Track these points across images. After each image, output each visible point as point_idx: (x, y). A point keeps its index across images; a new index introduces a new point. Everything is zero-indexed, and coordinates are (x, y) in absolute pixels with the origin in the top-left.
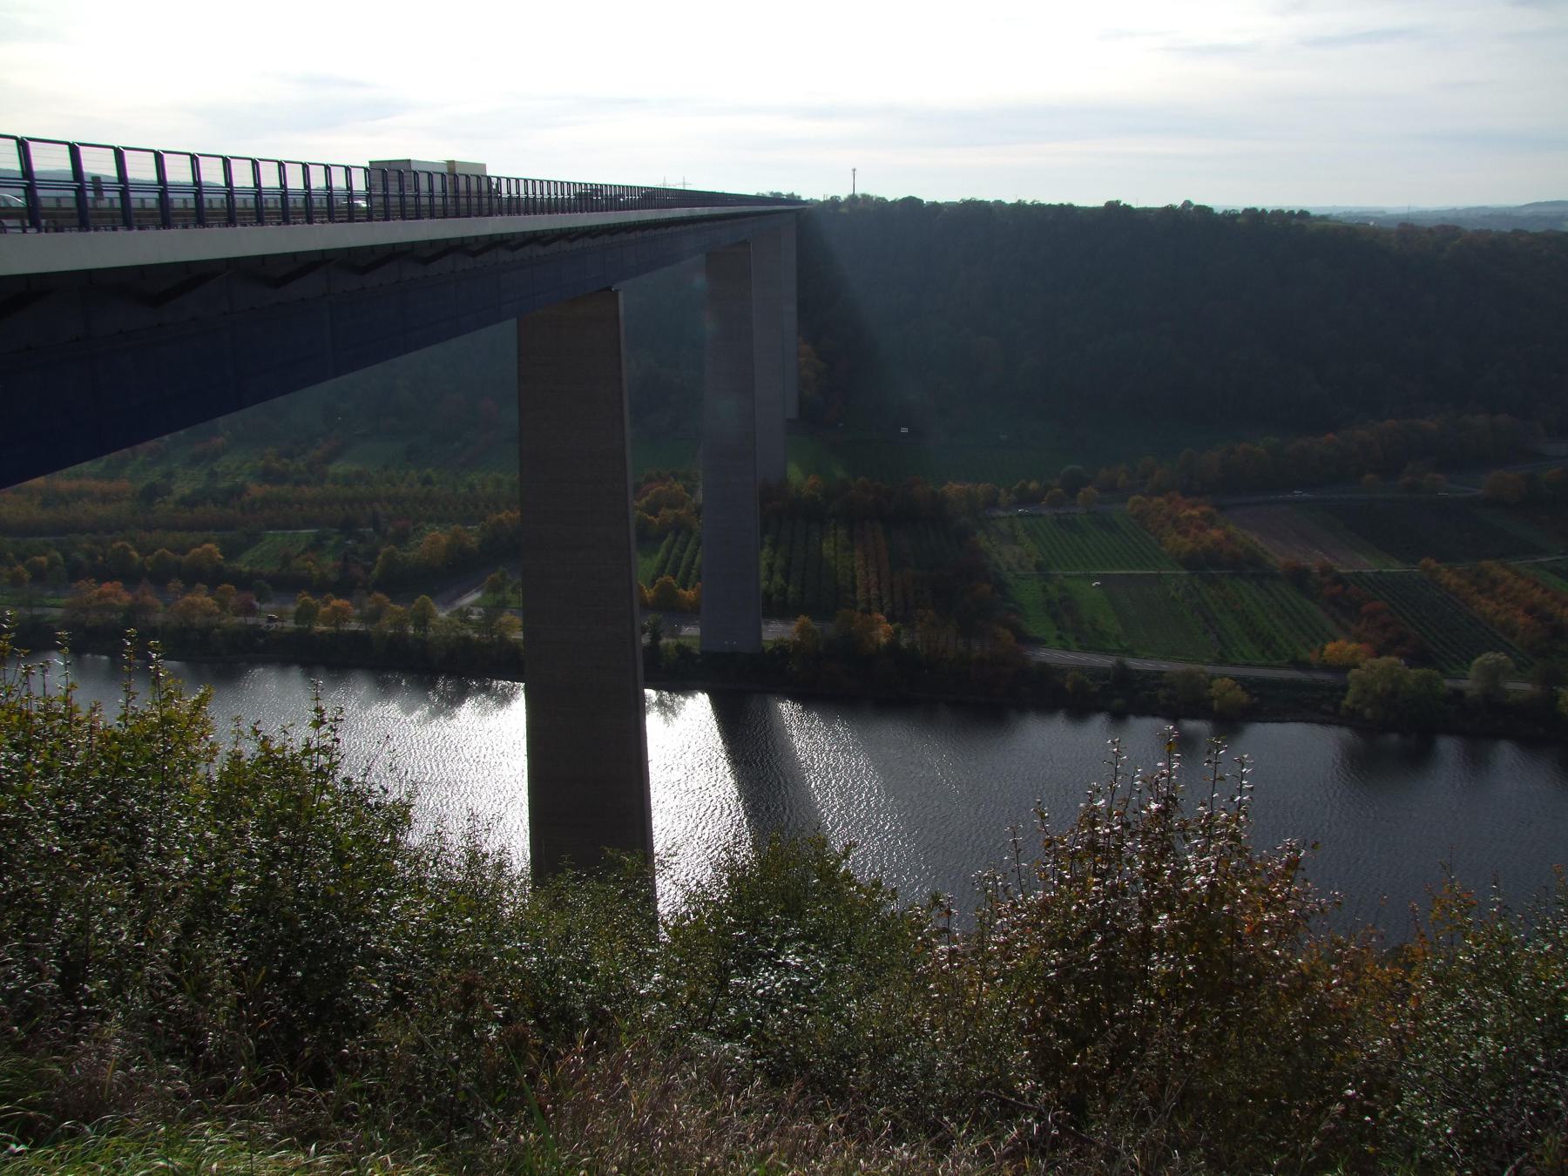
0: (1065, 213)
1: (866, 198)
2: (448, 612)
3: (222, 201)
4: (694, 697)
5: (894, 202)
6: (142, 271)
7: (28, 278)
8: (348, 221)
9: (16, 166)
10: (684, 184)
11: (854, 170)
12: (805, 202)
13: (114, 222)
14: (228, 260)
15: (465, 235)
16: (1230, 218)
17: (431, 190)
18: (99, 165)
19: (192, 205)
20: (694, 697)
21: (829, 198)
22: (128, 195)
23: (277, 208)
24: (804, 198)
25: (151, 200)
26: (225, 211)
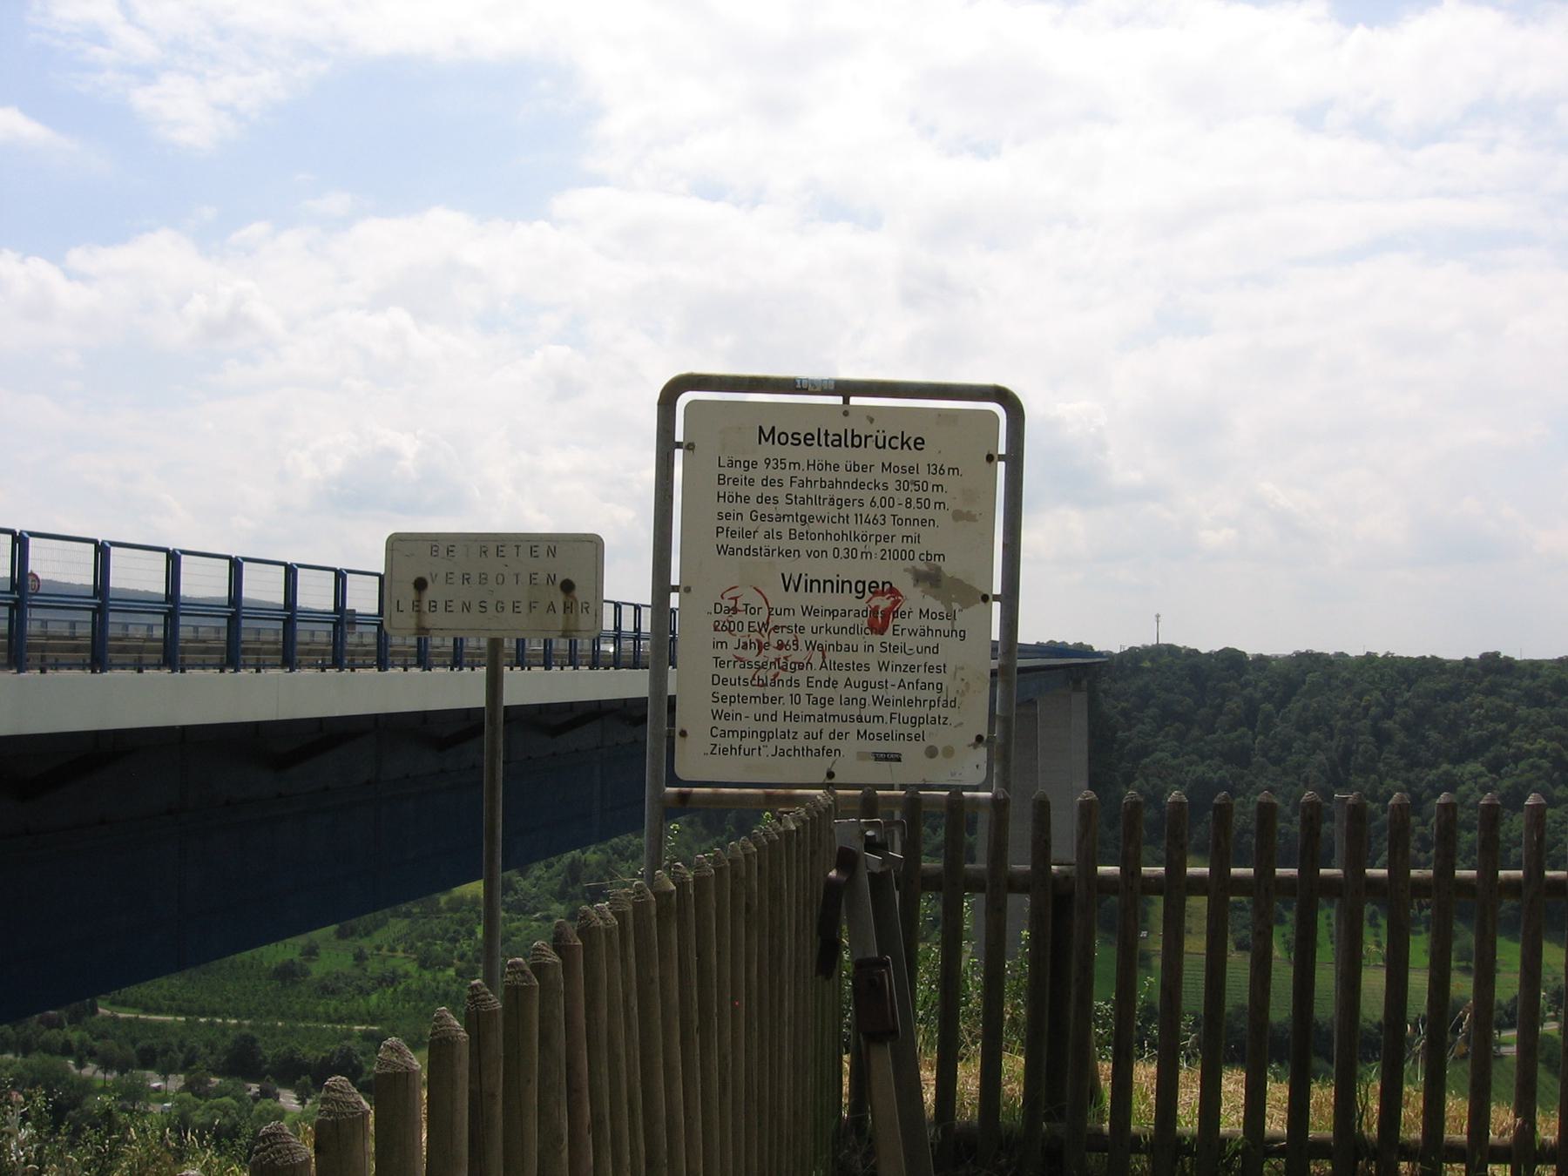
0: (1429, 667)
1: (1171, 649)
2: (1286, 914)
3: (218, 630)
4: (1499, 971)
5: (1210, 655)
6: (424, 718)
7: (320, 722)
8: (283, 666)
9: (160, 588)
10: (114, 567)
11: (1158, 616)
12: (1100, 654)
13: (43, 658)
14: (376, 717)
15: (601, 699)
16: (1417, 659)
17: (637, 629)
18: (263, 588)
19: (85, 630)
20: (1499, 971)
21: (1126, 649)
22: (239, 623)
23: (218, 639)
24: (1096, 649)
25: (272, 631)
26: (223, 645)
